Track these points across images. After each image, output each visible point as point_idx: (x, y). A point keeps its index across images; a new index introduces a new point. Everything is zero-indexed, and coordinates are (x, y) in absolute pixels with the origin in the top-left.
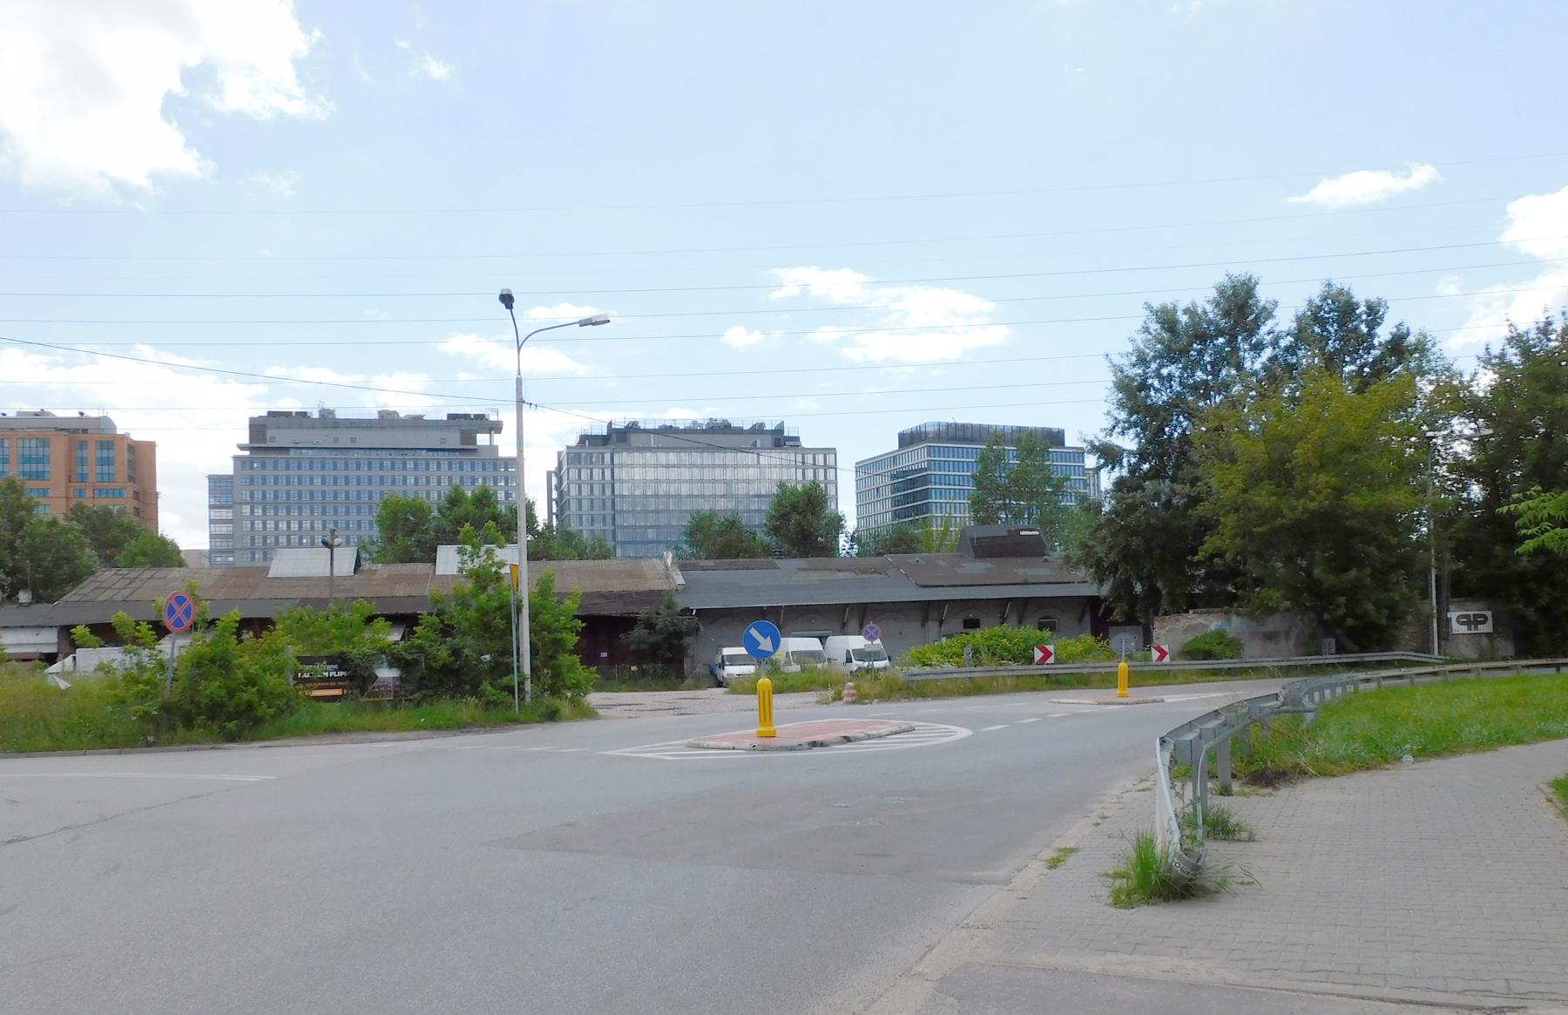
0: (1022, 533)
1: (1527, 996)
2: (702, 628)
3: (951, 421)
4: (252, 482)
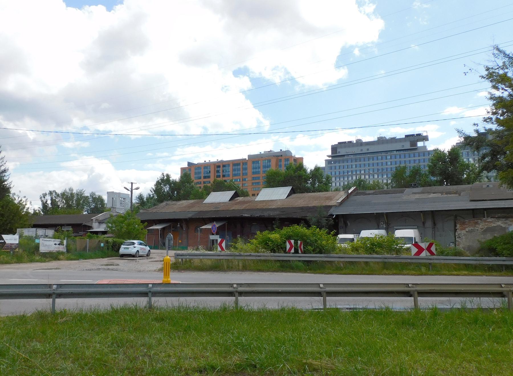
4: (331, 169)
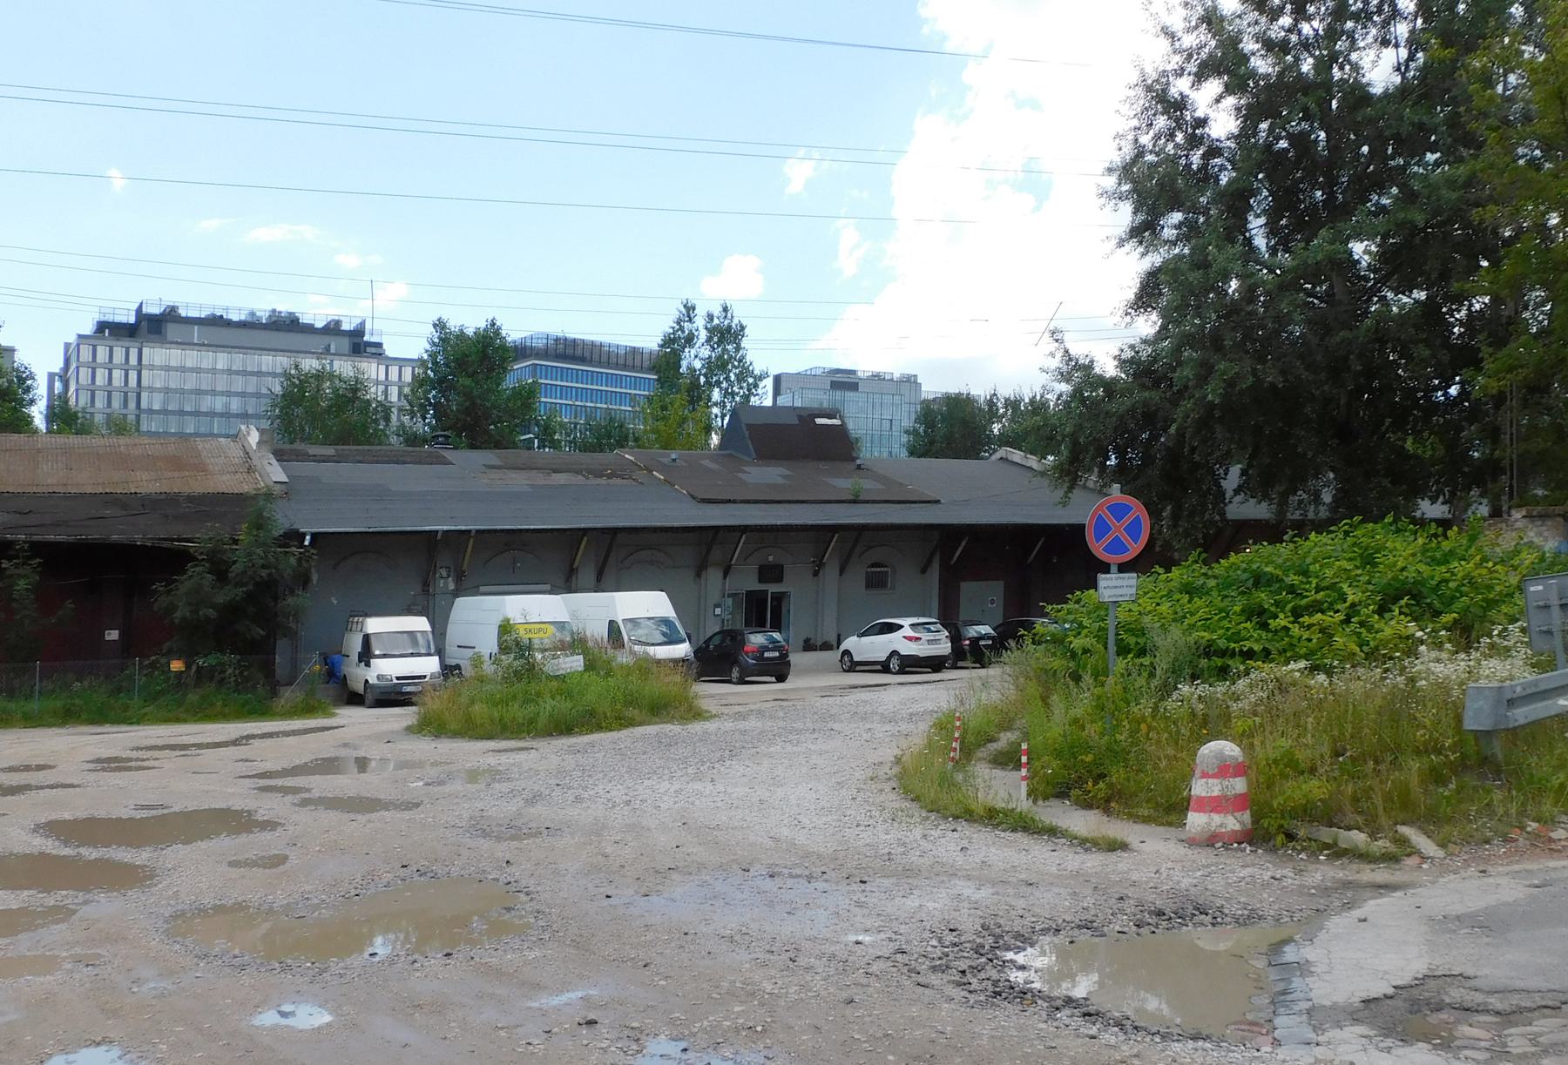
0: (819, 421)
1: (145, 764)
2: (315, 577)
3: (560, 335)
